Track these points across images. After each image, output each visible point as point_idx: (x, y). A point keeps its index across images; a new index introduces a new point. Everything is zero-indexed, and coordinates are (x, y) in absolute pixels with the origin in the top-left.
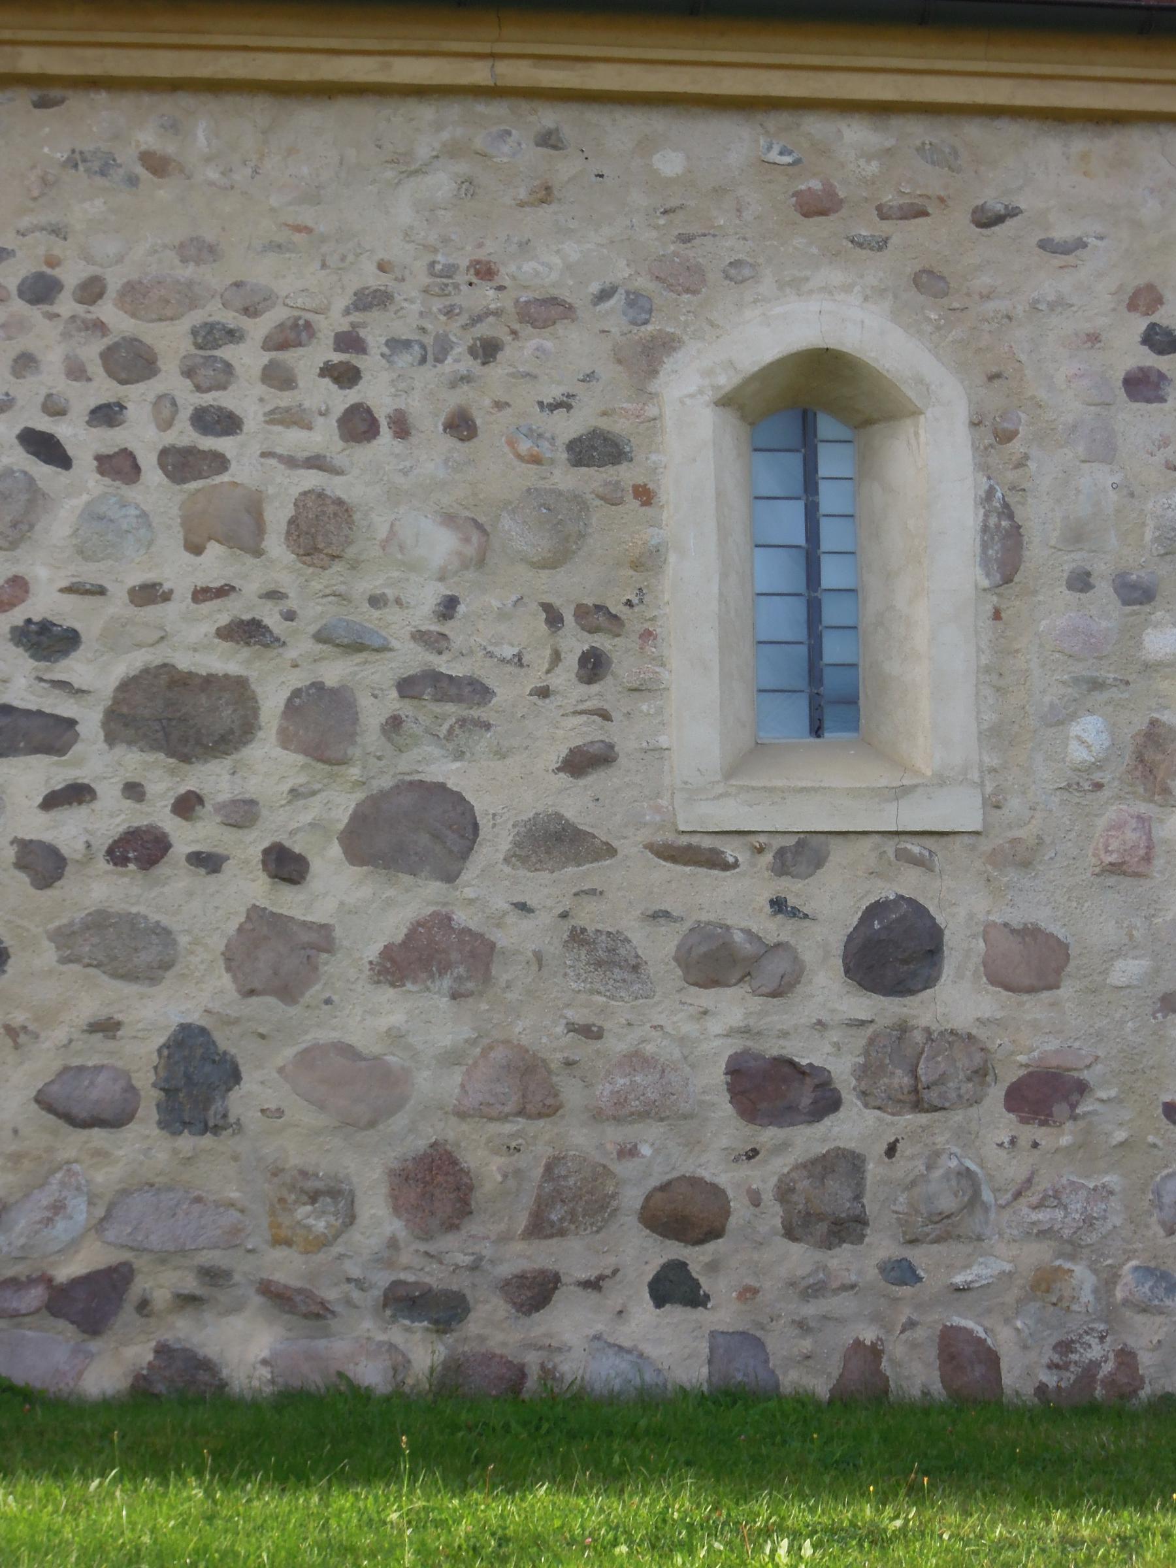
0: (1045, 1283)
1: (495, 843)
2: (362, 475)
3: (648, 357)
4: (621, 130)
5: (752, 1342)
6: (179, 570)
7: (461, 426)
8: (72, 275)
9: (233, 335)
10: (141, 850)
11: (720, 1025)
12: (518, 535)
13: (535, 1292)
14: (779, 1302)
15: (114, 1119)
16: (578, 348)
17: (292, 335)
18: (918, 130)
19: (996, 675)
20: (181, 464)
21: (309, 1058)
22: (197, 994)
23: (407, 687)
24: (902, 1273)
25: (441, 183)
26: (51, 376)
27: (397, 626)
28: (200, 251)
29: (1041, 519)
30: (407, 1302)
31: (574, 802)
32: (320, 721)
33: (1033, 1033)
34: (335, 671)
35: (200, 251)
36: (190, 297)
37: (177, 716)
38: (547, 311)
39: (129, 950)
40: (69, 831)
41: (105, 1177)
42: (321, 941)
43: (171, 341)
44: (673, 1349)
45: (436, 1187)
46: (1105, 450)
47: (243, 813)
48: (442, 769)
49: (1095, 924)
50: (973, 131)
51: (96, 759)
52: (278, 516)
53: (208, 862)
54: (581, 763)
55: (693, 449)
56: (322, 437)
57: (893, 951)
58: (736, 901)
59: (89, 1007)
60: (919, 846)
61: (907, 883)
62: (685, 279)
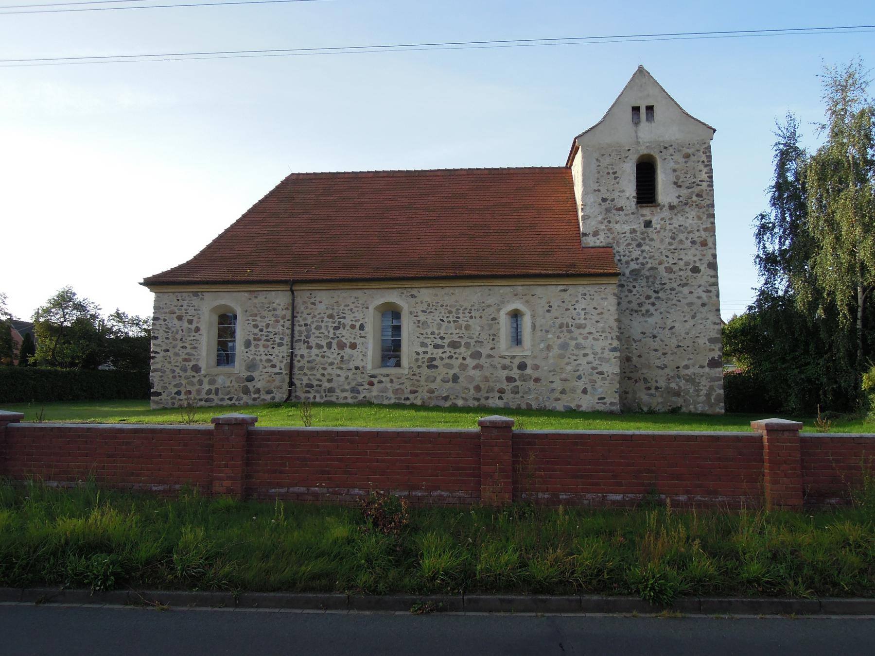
0: (537, 398)
1: (484, 356)
2: (472, 322)
3: (499, 310)
4: (496, 288)
5: (507, 403)
6: (454, 332)
7: (481, 317)
10: (451, 357)
11: (506, 373)
13: (487, 398)
15: (448, 382)
16: (492, 309)
20: (454, 322)
22: (456, 370)
24: (523, 397)
26: (443, 314)
27: (475, 336)
28: (457, 302)
29: (537, 324)
30: (475, 399)
31: (491, 352)
32: (467, 345)
33: (536, 374)
35: (457, 302)
37: (454, 345)
38: (489, 306)
39: (449, 366)
40: (444, 356)
43: (454, 310)
44: (500, 404)
45: (478, 388)
46: (544, 317)
47: (460, 354)
48: (480, 350)
51: (447, 349)
54: (492, 349)
55: (504, 320)
56: (468, 319)
57: (522, 366)
58: (507, 362)
61: (524, 360)
62: (503, 302)
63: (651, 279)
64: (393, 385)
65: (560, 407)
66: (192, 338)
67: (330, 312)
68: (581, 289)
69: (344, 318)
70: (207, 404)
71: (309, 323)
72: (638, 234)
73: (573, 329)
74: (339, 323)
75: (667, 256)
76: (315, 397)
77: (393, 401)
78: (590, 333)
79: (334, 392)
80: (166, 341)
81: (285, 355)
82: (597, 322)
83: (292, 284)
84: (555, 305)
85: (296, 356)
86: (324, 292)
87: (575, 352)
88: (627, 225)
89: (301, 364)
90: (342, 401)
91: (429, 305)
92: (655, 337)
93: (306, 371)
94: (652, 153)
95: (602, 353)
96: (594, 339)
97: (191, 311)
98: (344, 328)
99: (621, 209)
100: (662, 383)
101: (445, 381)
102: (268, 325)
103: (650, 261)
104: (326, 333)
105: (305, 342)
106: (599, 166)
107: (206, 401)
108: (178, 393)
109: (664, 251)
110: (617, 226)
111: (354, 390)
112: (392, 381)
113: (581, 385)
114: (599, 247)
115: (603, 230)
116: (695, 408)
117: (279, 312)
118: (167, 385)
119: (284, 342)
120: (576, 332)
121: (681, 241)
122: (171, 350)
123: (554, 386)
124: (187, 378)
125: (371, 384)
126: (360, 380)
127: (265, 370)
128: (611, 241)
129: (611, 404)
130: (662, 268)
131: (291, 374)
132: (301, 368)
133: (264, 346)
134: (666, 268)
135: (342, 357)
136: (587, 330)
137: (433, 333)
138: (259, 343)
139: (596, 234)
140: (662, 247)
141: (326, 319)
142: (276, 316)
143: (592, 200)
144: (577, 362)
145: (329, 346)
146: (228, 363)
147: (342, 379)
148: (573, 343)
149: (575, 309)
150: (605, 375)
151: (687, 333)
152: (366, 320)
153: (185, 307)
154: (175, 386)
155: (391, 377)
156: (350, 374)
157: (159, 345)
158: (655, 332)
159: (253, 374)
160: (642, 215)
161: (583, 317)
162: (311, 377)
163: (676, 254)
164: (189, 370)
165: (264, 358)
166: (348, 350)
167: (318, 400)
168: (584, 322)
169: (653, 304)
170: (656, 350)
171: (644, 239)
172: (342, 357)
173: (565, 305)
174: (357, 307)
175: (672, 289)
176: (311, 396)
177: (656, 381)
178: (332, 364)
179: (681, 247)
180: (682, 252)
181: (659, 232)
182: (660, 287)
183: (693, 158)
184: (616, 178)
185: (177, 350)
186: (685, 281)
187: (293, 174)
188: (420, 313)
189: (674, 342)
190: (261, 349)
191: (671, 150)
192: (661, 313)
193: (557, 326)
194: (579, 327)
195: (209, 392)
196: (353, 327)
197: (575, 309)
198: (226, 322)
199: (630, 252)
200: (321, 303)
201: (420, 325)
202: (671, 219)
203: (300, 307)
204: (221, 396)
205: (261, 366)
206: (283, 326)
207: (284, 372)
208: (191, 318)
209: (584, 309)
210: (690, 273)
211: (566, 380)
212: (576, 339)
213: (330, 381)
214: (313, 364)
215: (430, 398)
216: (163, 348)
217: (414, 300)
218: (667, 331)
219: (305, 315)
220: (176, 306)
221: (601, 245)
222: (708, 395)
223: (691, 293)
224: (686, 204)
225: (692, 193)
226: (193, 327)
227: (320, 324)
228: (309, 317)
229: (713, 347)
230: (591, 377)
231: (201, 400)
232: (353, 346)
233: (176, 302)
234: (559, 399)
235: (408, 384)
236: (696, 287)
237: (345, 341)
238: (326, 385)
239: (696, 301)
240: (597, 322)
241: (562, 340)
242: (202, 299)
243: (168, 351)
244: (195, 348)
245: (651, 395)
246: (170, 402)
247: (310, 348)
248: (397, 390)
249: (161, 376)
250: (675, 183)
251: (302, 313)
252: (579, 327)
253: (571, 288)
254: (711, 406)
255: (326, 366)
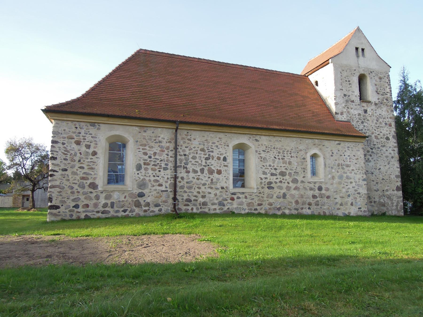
0: (328, 208)
1: (299, 182)
2: (292, 160)
3: (306, 153)
4: (304, 140)
5: (313, 212)
6: (283, 165)
7: (297, 157)
8: (276, 147)
9: (165, 161)
11: (311, 193)
12: (300, 164)
14: (316, 210)
16: (303, 153)
17: (288, 151)
18: (320, 140)
19: (325, 173)
21: (290, 194)
23: (294, 172)
24: (321, 208)
25: (295, 143)
26: (275, 153)
27: (294, 169)
29: (327, 163)
31: (303, 179)
32: (290, 174)
33: (327, 194)
34: (291, 171)
35: (282, 146)
36: (282, 149)
37: (283, 174)
38: (301, 150)
41: (280, 201)
42: (291, 187)
43: (281, 151)
44: (309, 212)
46: (330, 160)
47: (286, 180)
48: (296, 177)
49: (330, 187)
50: (323, 140)
51: (278, 176)
52: (287, 162)
53: (284, 183)
54: (304, 177)
56: (290, 157)
57: (320, 189)
58: (312, 185)
59: (279, 191)
60: (321, 182)
61: (321, 185)
62: (308, 149)
63: (369, 142)
64: (247, 200)
65: (340, 213)
66: (89, 160)
67: (201, 147)
68: (347, 144)
69: (212, 152)
70: (104, 216)
71: (187, 154)
72: (362, 116)
73: (344, 167)
74: (209, 155)
75: (375, 130)
76: (192, 209)
77: (247, 211)
78: (353, 170)
79: (207, 205)
80: (64, 161)
81: (169, 177)
82: (356, 163)
83: (176, 124)
84: (335, 152)
85: (178, 178)
86: (198, 132)
87: (346, 181)
88: (356, 111)
89: (181, 184)
90: (212, 212)
91: (266, 147)
92: (372, 173)
93: (185, 189)
94: (366, 74)
95: (359, 182)
96: (355, 173)
97: (89, 138)
98: (213, 159)
99: (353, 101)
100: (377, 199)
101: (278, 197)
102: (155, 154)
103: (368, 132)
104: (200, 162)
105: (184, 168)
106: (341, 76)
107: (103, 213)
108: (77, 206)
109: (374, 127)
110: (352, 111)
111: (221, 204)
112: (246, 197)
113: (350, 200)
114: (344, 121)
115: (345, 112)
116: (392, 213)
117: (164, 144)
118: (66, 199)
119: (169, 167)
120: (346, 169)
121: (381, 123)
122: (69, 169)
123: (337, 201)
124: (84, 193)
125: (232, 199)
126: (225, 197)
127: (154, 188)
128: (349, 119)
129: (364, 211)
130: (373, 136)
131: (175, 192)
132: (182, 187)
133: (152, 169)
134: (375, 136)
135: (212, 180)
136: (351, 168)
137: (270, 166)
138: (148, 167)
139: (342, 114)
140: (373, 125)
141: (199, 152)
142: (162, 147)
143: (339, 94)
144: (348, 187)
145: (202, 171)
146: (117, 182)
147: (212, 195)
148: (345, 175)
149: (345, 155)
150: (361, 195)
151: (386, 172)
152: (228, 154)
153: (83, 134)
154: (73, 200)
155: (247, 195)
156: (218, 192)
157: (58, 165)
158: (372, 171)
159: (144, 191)
160: (363, 107)
161: (349, 160)
162: (190, 194)
163: (379, 129)
164: (87, 187)
165: (152, 178)
166: (215, 175)
167: (195, 211)
168: (349, 163)
169: (371, 156)
170: (373, 181)
171: (364, 119)
172: (212, 180)
173: (340, 153)
174: (221, 145)
175: (378, 148)
176: (190, 208)
177: (374, 198)
178: (204, 184)
179: (381, 126)
180: (381, 128)
181: (371, 116)
182: (373, 146)
183: (383, 80)
184: (350, 84)
185: (75, 170)
186: (383, 144)
187: (141, 49)
188: (262, 152)
189: (381, 177)
190: (150, 172)
191: (374, 74)
192: (374, 161)
193: (337, 165)
194: (348, 166)
195: (105, 205)
196: (219, 158)
197: (345, 155)
198: (117, 148)
199: (359, 126)
200: (196, 140)
201: (262, 160)
202: (376, 110)
203: (180, 142)
204: (116, 209)
205: (150, 185)
206: (168, 155)
207: (169, 190)
208: (89, 143)
209: (349, 156)
210: (385, 140)
211: (343, 197)
212: (346, 173)
213: (203, 197)
214: (191, 185)
215: (270, 209)
216: (61, 168)
217: (257, 143)
218: (377, 171)
219: (184, 148)
220: (74, 133)
221: (345, 120)
222: (397, 206)
223: (387, 150)
224: (382, 103)
225: (384, 98)
226: (91, 151)
227: (196, 155)
228: (187, 150)
229: (397, 180)
230: (354, 196)
231: (98, 212)
232: (219, 172)
233: (74, 130)
234: (92, 159)
235: (256, 199)
236: (388, 148)
237: (213, 168)
238: (201, 200)
239: (389, 155)
240: (356, 163)
241: (340, 173)
242: (99, 129)
243: (66, 170)
244: (92, 168)
245: (372, 206)
246: (68, 214)
247: (188, 172)
248: (250, 203)
249: (60, 192)
250: (376, 92)
251: (181, 146)
252: (348, 166)
253: (342, 143)
254: (398, 211)
255: (201, 186)
